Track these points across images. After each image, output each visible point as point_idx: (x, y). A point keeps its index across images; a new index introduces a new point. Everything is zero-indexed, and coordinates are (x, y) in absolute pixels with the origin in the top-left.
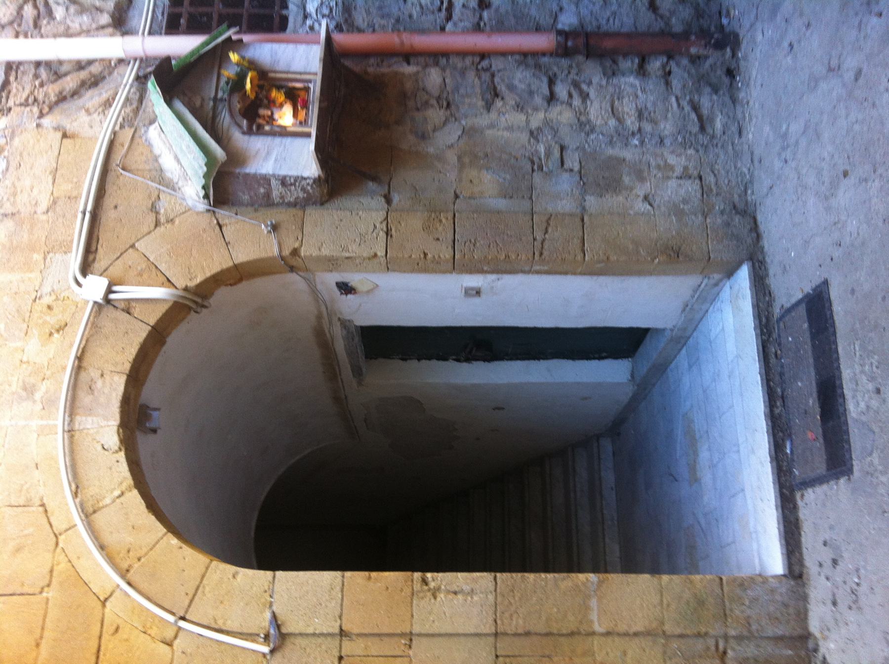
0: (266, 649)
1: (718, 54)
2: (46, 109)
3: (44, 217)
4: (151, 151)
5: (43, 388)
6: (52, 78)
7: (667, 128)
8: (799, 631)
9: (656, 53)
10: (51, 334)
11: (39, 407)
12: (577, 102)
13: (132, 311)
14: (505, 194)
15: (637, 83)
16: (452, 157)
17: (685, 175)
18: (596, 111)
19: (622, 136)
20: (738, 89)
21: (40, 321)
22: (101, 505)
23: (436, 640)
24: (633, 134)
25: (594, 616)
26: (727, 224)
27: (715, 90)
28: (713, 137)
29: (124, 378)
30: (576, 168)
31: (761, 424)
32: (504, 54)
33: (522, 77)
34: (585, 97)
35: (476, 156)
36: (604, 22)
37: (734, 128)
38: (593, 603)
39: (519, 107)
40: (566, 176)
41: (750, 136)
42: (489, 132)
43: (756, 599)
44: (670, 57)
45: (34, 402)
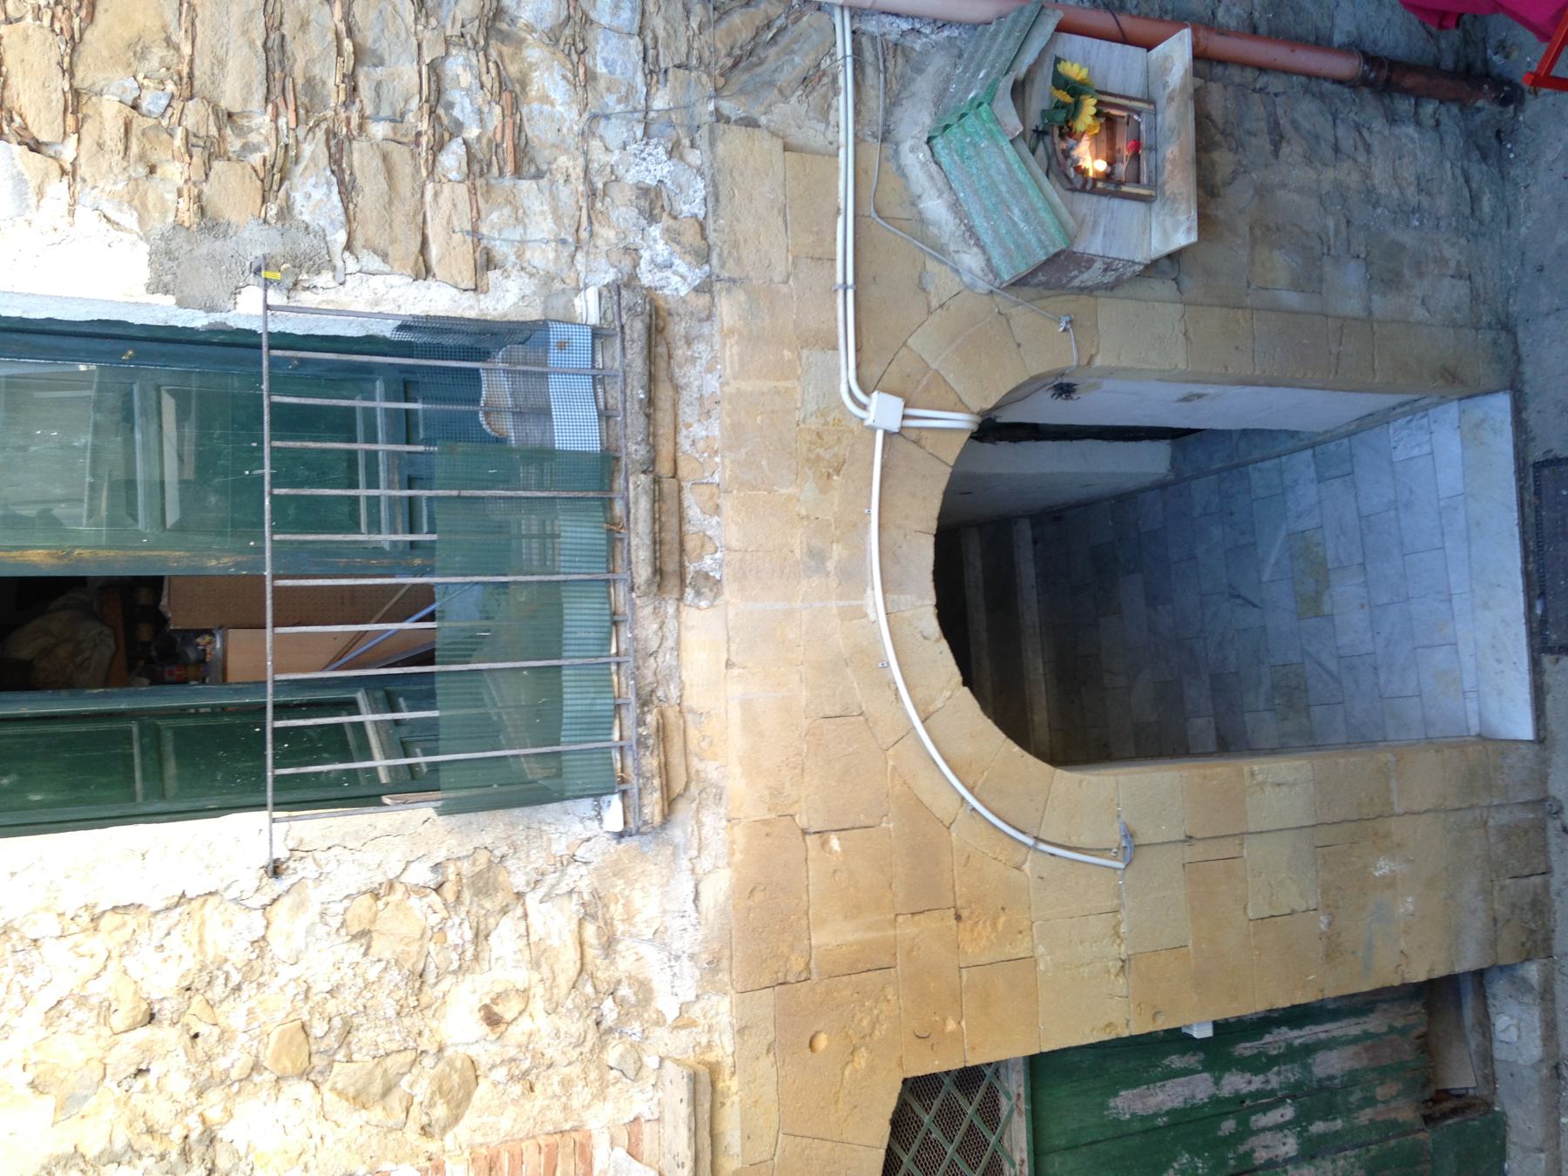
0: (1121, 865)
1: (1495, 108)
2: (1168, 18)
3: (784, 289)
4: (907, 189)
5: (837, 551)
6: (714, 16)
7: (1443, 205)
8: (1542, 795)
9: (1430, 96)
10: (829, 476)
11: (833, 583)
12: (1362, 158)
13: (923, 442)
14: (1296, 286)
15: (1416, 136)
16: (1243, 225)
17: (1459, 275)
18: (1380, 174)
19: (1404, 213)
20: (1510, 162)
21: (812, 456)
22: (931, 709)
23: (1266, 836)
24: (1413, 212)
25: (1394, 797)
26: (1495, 342)
27: (1484, 158)
28: (1481, 223)
29: (931, 540)
30: (1362, 251)
31: (1303, 393)
32: (1287, 72)
33: (1307, 111)
34: (1368, 149)
35: (1268, 228)
36: (1379, 34)
37: (1503, 216)
38: (1393, 783)
39: (1309, 159)
40: (1353, 264)
41: (1523, 230)
42: (1280, 193)
43: (1511, 767)
44: (1441, 102)
45: (828, 574)
